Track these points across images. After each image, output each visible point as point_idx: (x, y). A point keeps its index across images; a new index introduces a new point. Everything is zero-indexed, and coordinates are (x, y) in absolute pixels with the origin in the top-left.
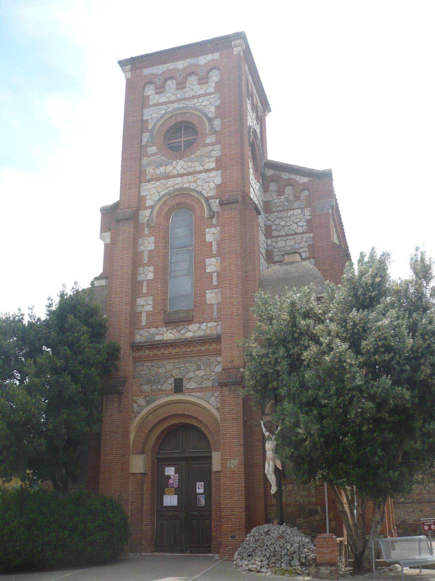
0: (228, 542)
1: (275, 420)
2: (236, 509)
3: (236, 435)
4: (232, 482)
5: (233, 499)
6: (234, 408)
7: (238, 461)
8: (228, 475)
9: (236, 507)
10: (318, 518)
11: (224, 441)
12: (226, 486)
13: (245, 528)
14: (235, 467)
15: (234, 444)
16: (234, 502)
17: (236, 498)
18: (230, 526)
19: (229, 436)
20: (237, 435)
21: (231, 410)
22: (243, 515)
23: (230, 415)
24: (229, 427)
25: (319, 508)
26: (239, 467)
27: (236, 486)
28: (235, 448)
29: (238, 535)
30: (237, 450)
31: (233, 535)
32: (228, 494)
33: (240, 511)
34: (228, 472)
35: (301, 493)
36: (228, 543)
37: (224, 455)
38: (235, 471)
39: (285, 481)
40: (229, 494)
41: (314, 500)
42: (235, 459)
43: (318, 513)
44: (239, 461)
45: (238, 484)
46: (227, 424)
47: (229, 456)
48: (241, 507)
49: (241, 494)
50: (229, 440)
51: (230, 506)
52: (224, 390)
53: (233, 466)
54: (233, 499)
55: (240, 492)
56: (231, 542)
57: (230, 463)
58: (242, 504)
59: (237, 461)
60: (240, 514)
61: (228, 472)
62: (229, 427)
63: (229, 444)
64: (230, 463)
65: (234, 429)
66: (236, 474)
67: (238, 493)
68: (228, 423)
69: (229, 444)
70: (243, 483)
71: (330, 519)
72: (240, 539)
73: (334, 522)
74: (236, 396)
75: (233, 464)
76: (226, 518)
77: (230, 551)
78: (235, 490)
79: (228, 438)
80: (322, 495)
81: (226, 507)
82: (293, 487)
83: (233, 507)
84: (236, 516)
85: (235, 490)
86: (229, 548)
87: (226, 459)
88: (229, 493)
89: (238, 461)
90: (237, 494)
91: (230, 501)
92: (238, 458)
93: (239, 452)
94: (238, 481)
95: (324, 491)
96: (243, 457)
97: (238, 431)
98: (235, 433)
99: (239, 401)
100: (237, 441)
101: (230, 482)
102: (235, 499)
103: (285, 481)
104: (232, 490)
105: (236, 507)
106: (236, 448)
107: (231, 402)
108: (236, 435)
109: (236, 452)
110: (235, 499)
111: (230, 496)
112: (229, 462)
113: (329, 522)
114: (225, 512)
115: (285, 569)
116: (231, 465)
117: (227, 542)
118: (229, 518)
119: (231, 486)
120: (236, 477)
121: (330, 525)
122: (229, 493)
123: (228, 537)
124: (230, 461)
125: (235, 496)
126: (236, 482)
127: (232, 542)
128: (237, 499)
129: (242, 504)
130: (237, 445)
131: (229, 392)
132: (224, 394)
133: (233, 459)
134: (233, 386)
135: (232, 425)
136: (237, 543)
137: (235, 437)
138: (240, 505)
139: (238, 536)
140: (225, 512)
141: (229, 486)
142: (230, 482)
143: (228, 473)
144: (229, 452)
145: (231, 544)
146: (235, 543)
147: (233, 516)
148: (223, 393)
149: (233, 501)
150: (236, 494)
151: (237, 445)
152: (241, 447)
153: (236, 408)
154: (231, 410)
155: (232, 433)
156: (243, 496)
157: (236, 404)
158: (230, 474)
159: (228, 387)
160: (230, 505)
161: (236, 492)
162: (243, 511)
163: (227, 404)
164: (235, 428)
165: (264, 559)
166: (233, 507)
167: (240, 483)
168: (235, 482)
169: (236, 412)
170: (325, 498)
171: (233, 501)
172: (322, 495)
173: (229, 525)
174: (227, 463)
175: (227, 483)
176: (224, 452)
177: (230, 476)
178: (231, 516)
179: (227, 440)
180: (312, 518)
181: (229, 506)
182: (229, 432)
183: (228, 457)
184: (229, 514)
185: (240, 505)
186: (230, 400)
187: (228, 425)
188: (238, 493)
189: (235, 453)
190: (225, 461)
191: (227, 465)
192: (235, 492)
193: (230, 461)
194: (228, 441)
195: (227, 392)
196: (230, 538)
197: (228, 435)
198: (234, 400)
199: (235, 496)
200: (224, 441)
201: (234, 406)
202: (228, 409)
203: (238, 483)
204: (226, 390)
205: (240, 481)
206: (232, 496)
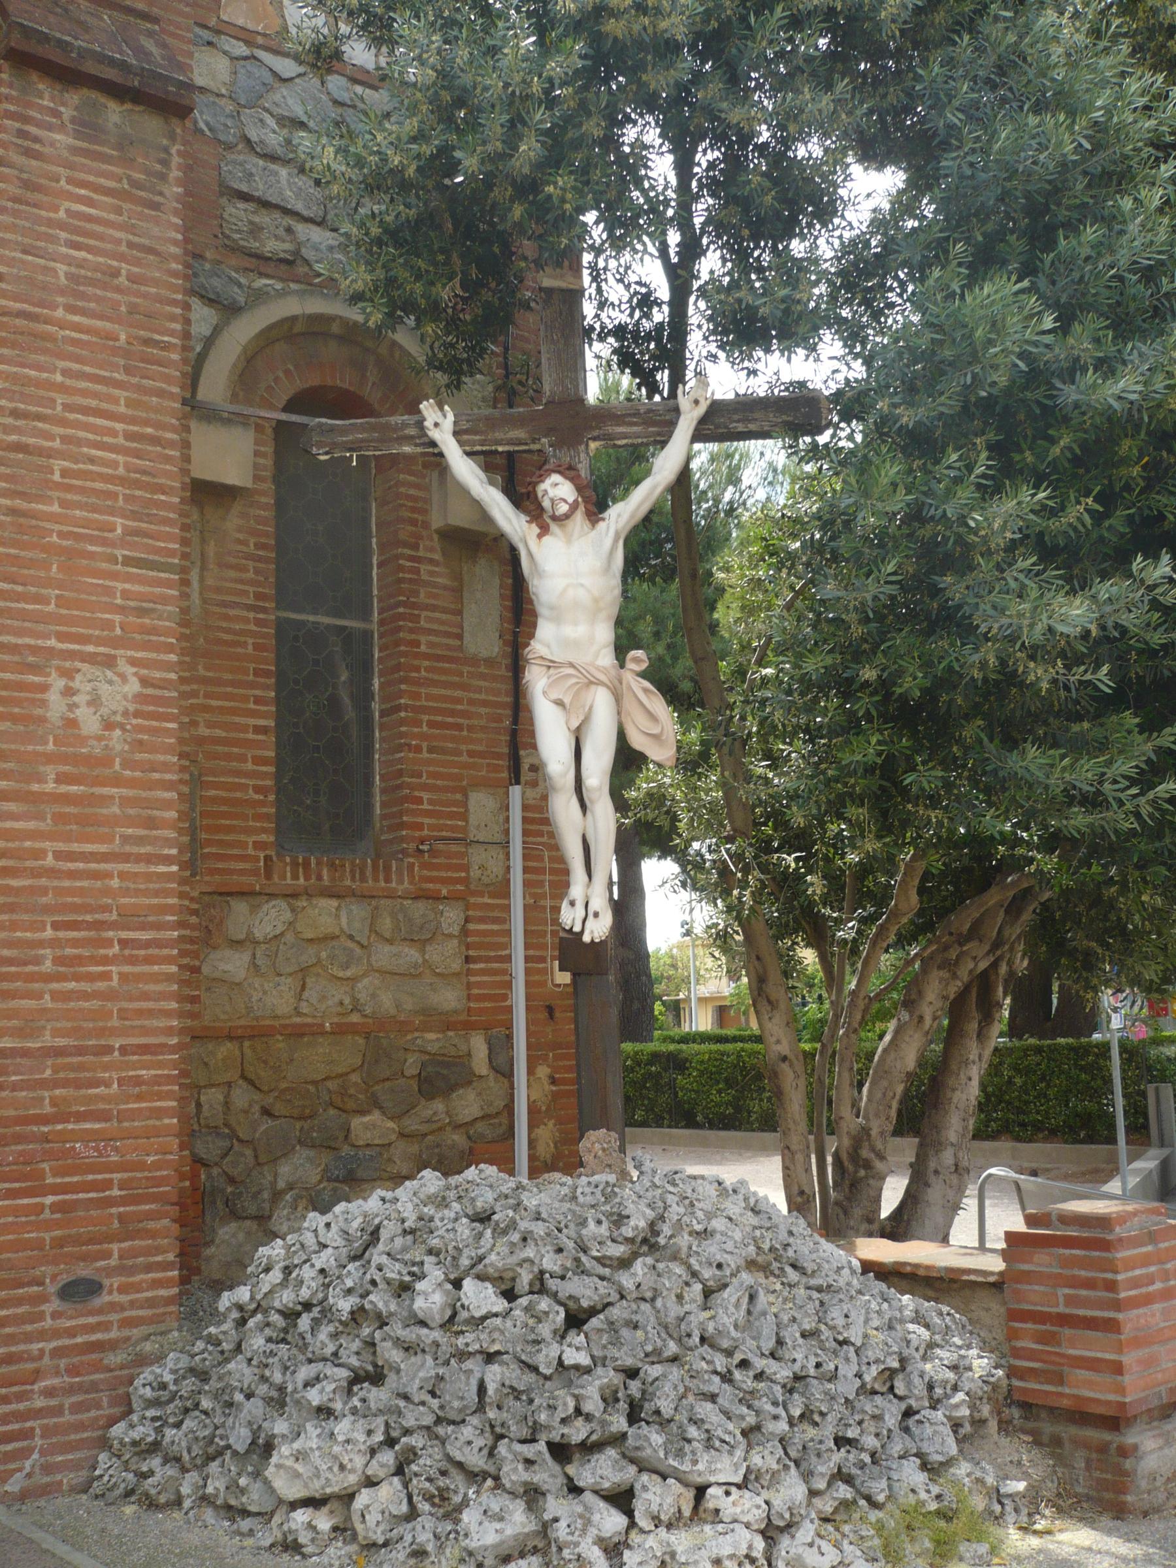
0: (42, 1335)
1: (858, 349)
2: (106, 1067)
3: (122, 481)
4: (75, 847)
5: (84, 986)
6: (116, 273)
7: (134, 686)
8: (50, 786)
9: (109, 1050)
10: (468, 1104)
11: (18, 503)
12: (36, 873)
13: (174, 1211)
14: (109, 725)
15: (104, 542)
16: (95, 1004)
17: (106, 976)
18: (55, 1207)
19: (65, 473)
20: (137, 484)
21: (92, 282)
22: (159, 1113)
23: (83, 312)
24: (67, 407)
25: (479, 1046)
26: (139, 729)
27: (115, 883)
28: (114, 576)
29: (121, 1270)
30: (126, 594)
31: (83, 1271)
32: (41, 944)
33: (138, 1081)
34: (49, 759)
35: (384, 955)
36: (36, 1347)
37: (23, 615)
38: (107, 761)
39: (295, 877)
40: (54, 943)
41: (449, 998)
42: (109, 662)
43: (469, 1079)
44: (144, 682)
45: (127, 867)
46: (59, 378)
47: (61, 637)
48: (144, 1049)
49: (148, 944)
50: (63, 504)
51: (61, 1042)
52: (41, 108)
53: (90, 723)
54: (84, 986)
55: (143, 927)
56: (56, 1334)
57: (69, 692)
58: (162, 1023)
59: (123, 677)
60: (139, 1098)
61: (49, 759)
62: (67, 407)
63: (61, 535)
64: (69, 692)
65: (113, 433)
66: (117, 781)
67: (124, 935)
68: (65, 372)
69: (61, 535)
70: (168, 860)
71: (533, 1110)
72: (133, 1304)
73: (551, 1124)
74: (134, 183)
75: (95, 702)
76: (19, 1139)
77: (58, 1411)
78: (106, 909)
79: (59, 486)
80: (495, 972)
81: (25, 1053)
82: (337, 916)
83: (81, 1051)
84: (104, 1116)
85: (106, 909)
86: (49, 1393)
87: (35, 650)
88: (49, 933)
89: (134, 686)
90: (123, 943)
91: (56, 996)
92: (133, 662)
93: (141, 612)
94: (125, 839)
95: (507, 945)
96: (173, 657)
97: (138, 454)
98: (114, 464)
99: (156, 231)
100: (128, 532)
101: (61, 846)
102: (101, 985)
103: (295, 877)
104: (75, 908)
105: (109, 1050)
106: (129, 578)
107: (90, 219)
108: (122, 481)
109: (121, 610)
110: (101, 985)
111: (58, 961)
112: (60, 683)
113: (531, 1127)
114: (15, 1087)
115: (933, 1506)
116: (72, 707)
117: (29, 1338)
118: (46, 1139)
119: (72, 875)
120: (115, 809)
121: (532, 1144)
122: (49, 933)
123: (43, 1299)
124: (68, 674)
125: (105, 960)
126: (116, 846)
127: (71, 1333)
128: (115, 982)
129: (162, 1023)
130: (127, 561)
131: (78, 135)
132: (36, 139)
133: (91, 659)
134: (112, 105)
135: (95, 395)
136: (114, 1334)
137: (114, 496)
138: (145, 1031)
139: (116, 1281)
140: (15, 1087)
141: (52, 873)
142: (61, 846)
143: (50, 771)
144: (61, 601)
145: (57, 1353)
146: (99, 1336)
147: (80, 1117)
148: (33, 130)
149: (86, 996)
150: (108, 943)
151: (127, 561)
152: (160, 583)
153: (132, 278)
154: (92, 282)
155: (92, 460)
156: (168, 960)
157: (130, 245)
158: (60, 779)
159: (74, 98)
160: (56, 1033)
161: (113, 926)
162: (169, 1079)
163: (62, 226)
164: (119, 426)
165: (765, 1458)
166: (81, 1051)
167: (149, 859)
168: (103, 848)
169: (133, 309)
170: (509, 985)
171: (86, 996)
172: (495, 972)
173: (49, 1200)
174: (44, 688)
175: (39, 854)
176: (20, 597)
177: (66, 799)
178: (64, 1118)
179: (49, 500)
180: (439, 1106)
181: (48, 1040)
182: (65, 439)
183: (52, 642)
184: (48, 1109)
185: (145, 1031)
186: (90, 203)
187: (62, 388)
188: (124, 935)
189: (117, 618)
190: (34, 669)
191: (44, 703)
192: (99, 925)
193: (68, 674)
194: (56, 508)
195: (62, 128)
196: (55, 1304)
197: (58, 464)
198: (118, 211)
199: (105, 960)
200: (18, 503)
201: (122, 258)
202: (68, 261)
203: (126, 858)
204: (56, 114)
205: (140, 840)
206: (79, 960)
